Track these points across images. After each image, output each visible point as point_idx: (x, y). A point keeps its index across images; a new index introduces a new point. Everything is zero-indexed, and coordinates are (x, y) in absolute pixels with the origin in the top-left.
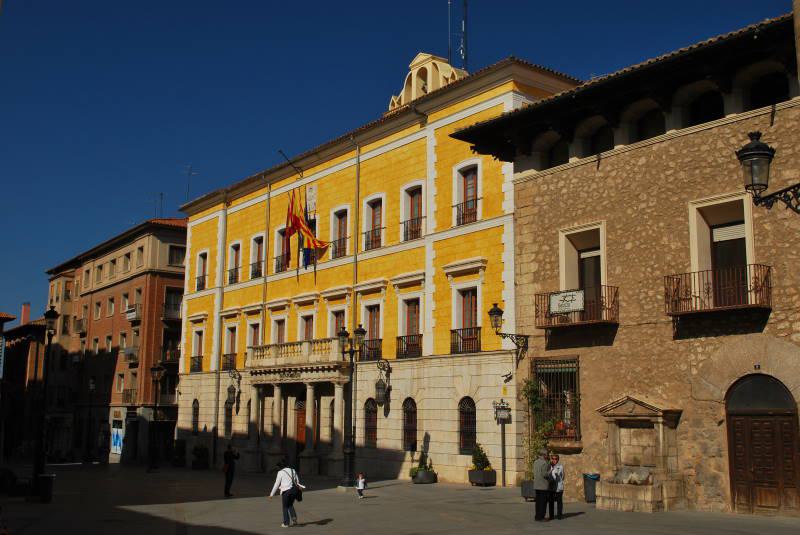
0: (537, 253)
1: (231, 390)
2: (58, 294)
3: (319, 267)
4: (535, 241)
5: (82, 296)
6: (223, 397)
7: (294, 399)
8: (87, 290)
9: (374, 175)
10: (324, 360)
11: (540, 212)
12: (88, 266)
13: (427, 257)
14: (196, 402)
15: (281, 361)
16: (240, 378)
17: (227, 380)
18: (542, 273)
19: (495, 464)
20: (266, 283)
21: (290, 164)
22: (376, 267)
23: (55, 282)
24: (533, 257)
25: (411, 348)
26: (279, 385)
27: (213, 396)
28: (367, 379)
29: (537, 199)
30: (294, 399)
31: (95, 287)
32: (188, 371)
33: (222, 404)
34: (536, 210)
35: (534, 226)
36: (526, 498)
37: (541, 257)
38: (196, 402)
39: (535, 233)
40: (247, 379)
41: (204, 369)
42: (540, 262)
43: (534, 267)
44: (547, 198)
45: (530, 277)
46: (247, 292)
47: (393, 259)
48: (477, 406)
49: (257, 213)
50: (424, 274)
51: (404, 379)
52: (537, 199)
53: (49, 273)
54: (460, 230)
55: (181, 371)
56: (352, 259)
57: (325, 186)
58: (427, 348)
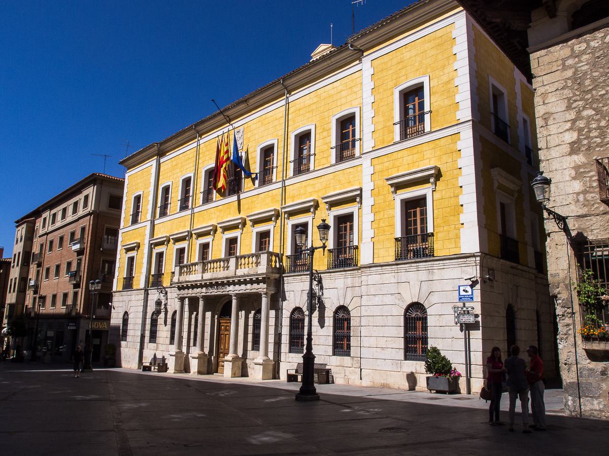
0: (574, 121)
1: (158, 303)
2: (22, 236)
3: (242, 196)
4: (569, 108)
5: (40, 237)
6: (151, 308)
7: (210, 313)
8: (44, 232)
9: (301, 112)
10: (252, 273)
11: (574, 73)
12: (46, 214)
13: (363, 174)
14: (126, 313)
15: (207, 276)
16: (166, 293)
17: (154, 295)
18: (585, 142)
19: (457, 362)
20: (193, 214)
21: (221, 113)
22: (302, 190)
23: (20, 228)
24: (569, 125)
25: (343, 257)
26: (203, 297)
27: (141, 309)
28: (296, 290)
29: (570, 62)
30: (210, 313)
31: (51, 229)
32: (121, 289)
33: (149, 315)
34: (569, 73)
35: (566, 91)
36: (431, 390)
37: (581, 124)
38: (126, 313)
39: (569, 99)
40: (173, 294)
41: (135, 287)
42: (580, 130)
43: (572, 136)
44: (585, 57)
45: (566, 148)
46: (175, 223)
47: (326, 179)
48: (429, 311)
49: (191, 160)
50: (361, 190)
51: (337, 289)
52: (570, 62)
53: (17, 222)
54: (404, 143)
55: (114, 289)
56: (280, 185)
57: (259, 129)
58: (365, 257)
